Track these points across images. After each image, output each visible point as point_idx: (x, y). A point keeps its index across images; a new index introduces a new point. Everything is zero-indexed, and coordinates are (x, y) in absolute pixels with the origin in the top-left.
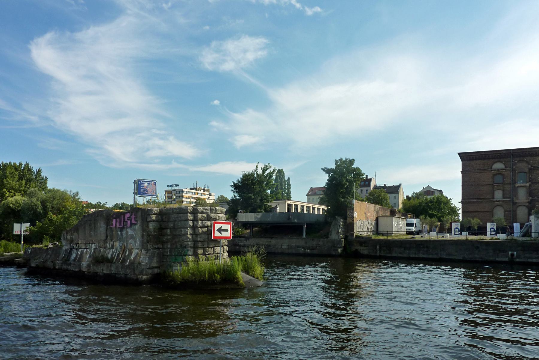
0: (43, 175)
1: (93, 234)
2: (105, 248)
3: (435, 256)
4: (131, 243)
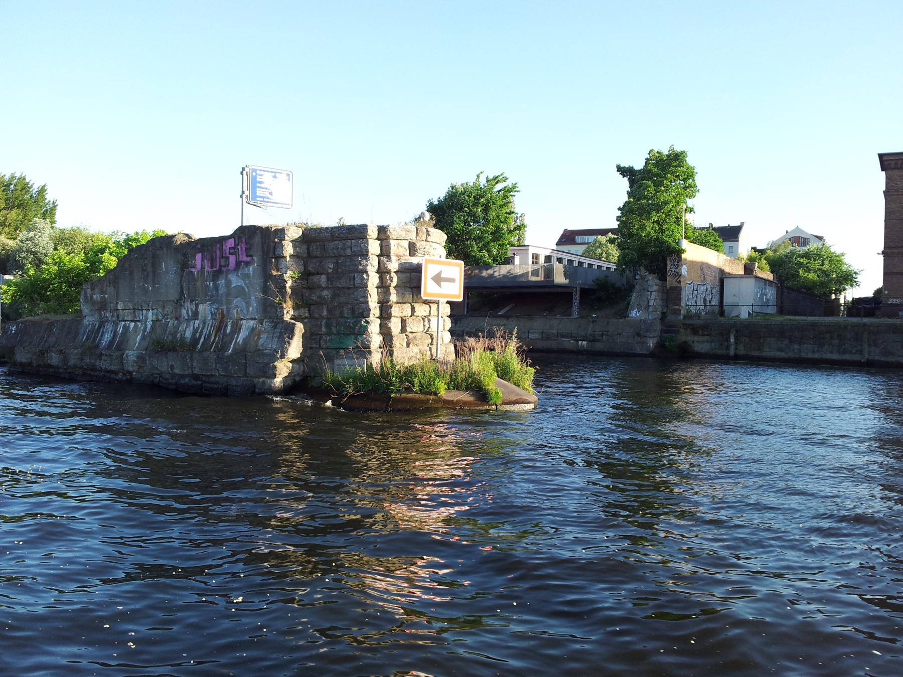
0: (50, 197)
1: (150, 288)
2: (177, 319)
3: (856, 357)
4: (237, 306)
